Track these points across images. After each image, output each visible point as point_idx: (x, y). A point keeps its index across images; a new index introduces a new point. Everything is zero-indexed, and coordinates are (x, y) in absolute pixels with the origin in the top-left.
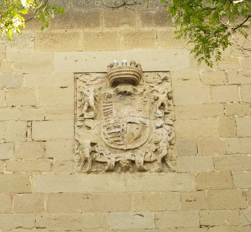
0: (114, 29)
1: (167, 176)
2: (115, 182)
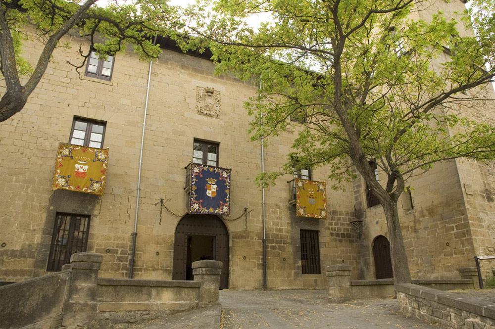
0: (207, 76)
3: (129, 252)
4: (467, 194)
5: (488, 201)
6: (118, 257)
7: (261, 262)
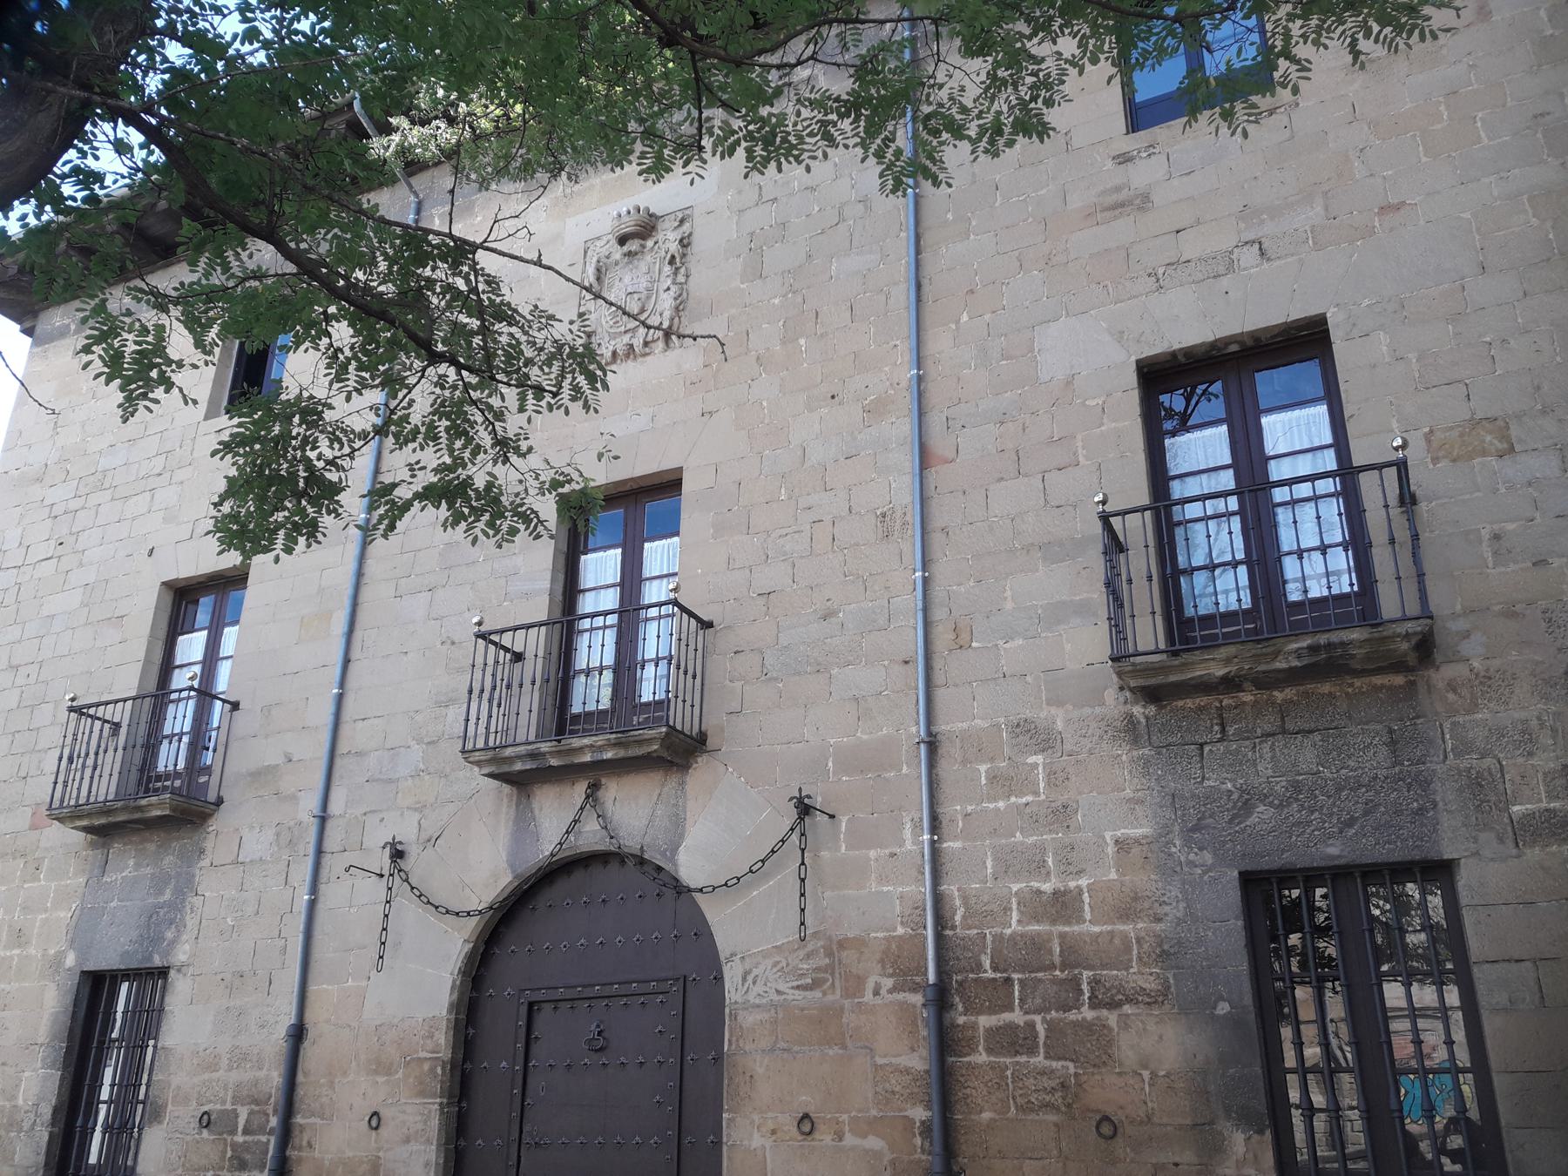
6: (234, 1146)
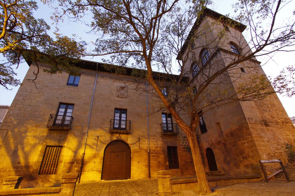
1: (126, 99)
2: (120, 99)
3: (80, 163)
4: (250, 123)
5: (265, 126)
7: (147, 164)
